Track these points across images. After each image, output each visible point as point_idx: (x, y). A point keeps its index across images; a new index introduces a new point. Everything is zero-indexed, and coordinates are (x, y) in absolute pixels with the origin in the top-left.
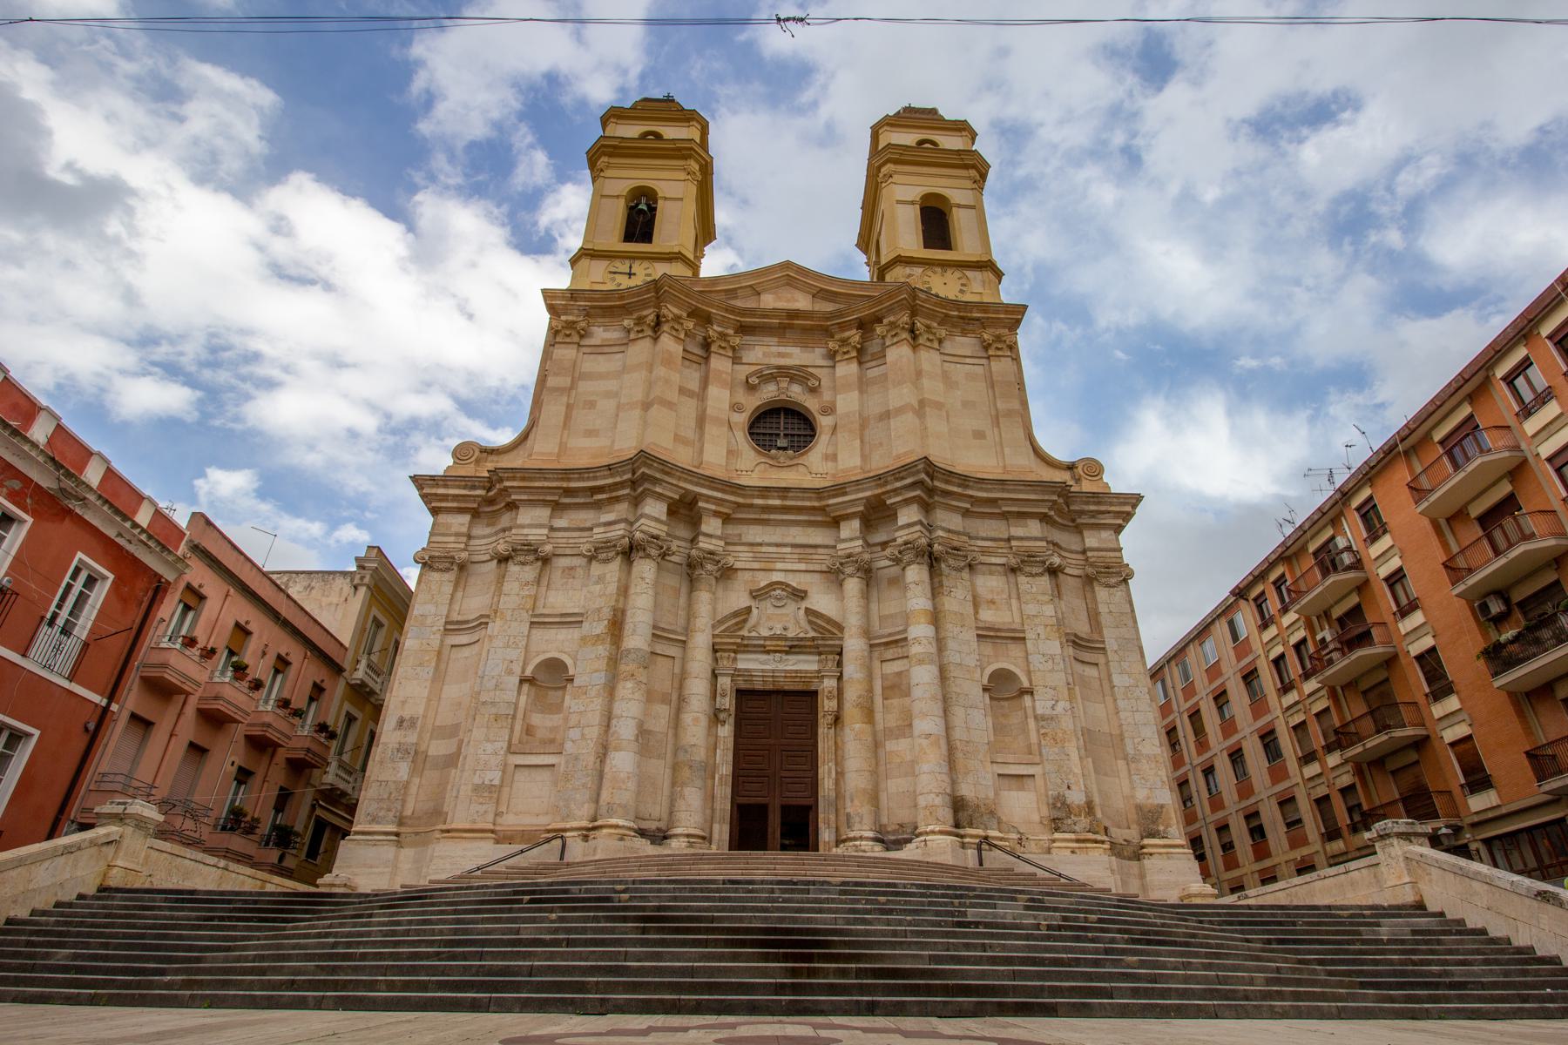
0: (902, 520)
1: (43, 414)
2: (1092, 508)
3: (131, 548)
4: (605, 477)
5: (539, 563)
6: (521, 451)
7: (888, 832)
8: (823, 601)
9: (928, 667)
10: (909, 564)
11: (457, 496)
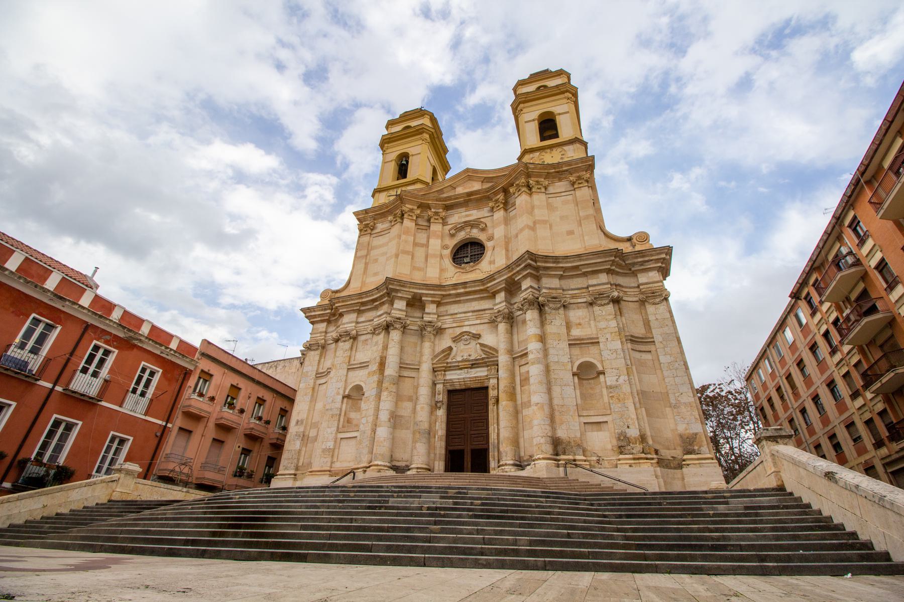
0: (524, 287)
1: (117, 307)
2: (640, 260)
3: (169, 358)
4: (376, 294)
5: (352, 340)
6: (347, 289)
7: (524, 461)
8: (489, 339)
9: (537, 366)
10: (527, 310)
11: (320, 314)
